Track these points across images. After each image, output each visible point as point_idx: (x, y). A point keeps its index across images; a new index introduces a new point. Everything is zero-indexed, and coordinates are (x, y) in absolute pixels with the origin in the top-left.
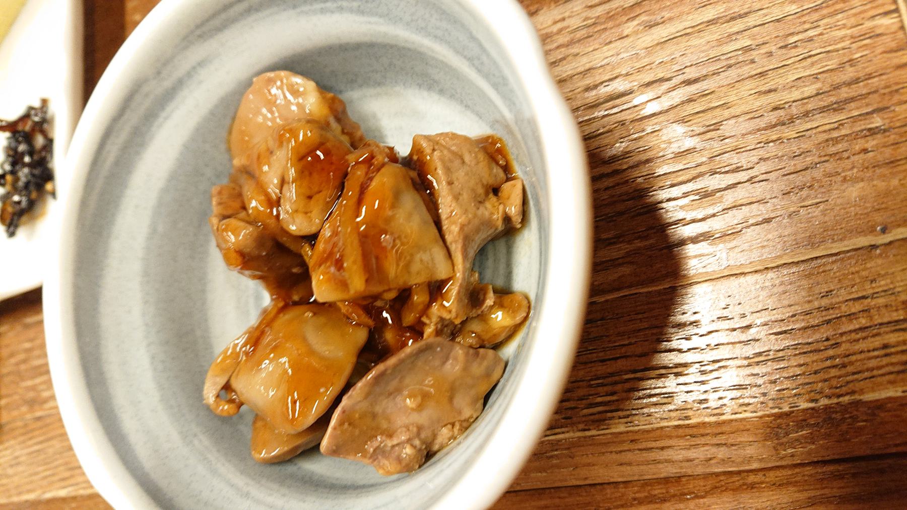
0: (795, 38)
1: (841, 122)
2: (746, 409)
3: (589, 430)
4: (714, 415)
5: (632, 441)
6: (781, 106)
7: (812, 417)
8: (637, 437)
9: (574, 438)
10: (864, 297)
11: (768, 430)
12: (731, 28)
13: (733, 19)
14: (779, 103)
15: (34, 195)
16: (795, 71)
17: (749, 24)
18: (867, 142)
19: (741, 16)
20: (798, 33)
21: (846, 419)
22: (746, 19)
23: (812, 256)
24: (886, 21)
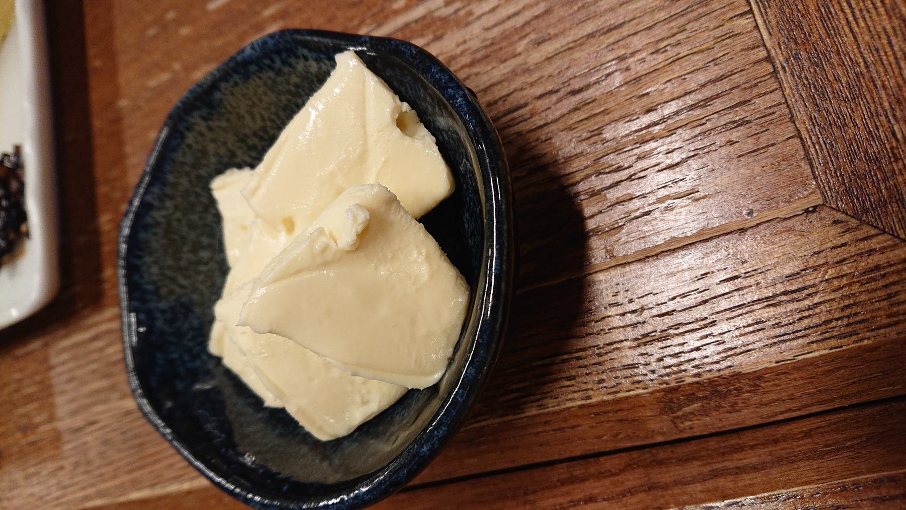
0: (665, 43)
1: (707, 118)
2: (638, 386)
3: (507, 415)
4: (611, 393)
5: (545, 423)
6: (654, 108)
7: (699, 390)
8: (549, 419)
9: (563, 483)
10: (736, 277)
11: (662, 405)
12: (607, 39)
13: (610, 30)
14: (651, 105)
15: (12, 236)
16: (665, 74)
17: (623, 35)
18: (731, 134)
19: (616, 28)
20: (667, 38)
21: (731, 390)
22: (621, 30)
23: (686, 243)
24: (743, 22)
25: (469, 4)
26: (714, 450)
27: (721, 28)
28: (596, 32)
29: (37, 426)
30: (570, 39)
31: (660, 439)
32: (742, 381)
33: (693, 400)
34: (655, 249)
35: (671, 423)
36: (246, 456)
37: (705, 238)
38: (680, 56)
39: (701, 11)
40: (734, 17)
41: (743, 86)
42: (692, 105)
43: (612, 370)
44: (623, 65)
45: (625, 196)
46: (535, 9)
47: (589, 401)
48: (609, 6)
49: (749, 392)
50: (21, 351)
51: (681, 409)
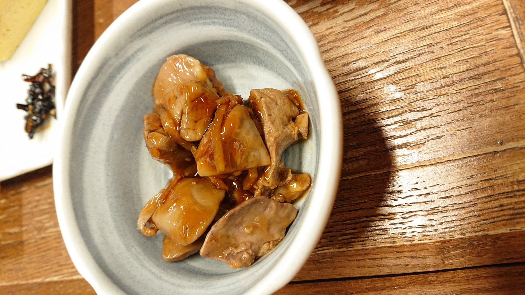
0: (456, 40)
1: (479, 85)
6: (448, 76)
7: (462, 243)
8: (368, 252)
13: (423, 29)
14: (447, 74)
17: (431, 32)
21: (480, 244)
22: (430, 29)
24: (504, 32)
25: (336, 6)
26: (462, 277)
27: (490, 35)
28: (415, 28)
29: (47, 228)
30: (398, 31)
31: (432, 269)
32: (488, 239)
33: (457, 248)
34: (444, 159)
35: (441, 260)
36: (145, 115)
37: (474, 155)
38: (465, 48)
39: (479, 23)
40: (499, 29)
41: (502, 69)
42: (471, 77)
43: (410, 227)
44: (431, 49)
45: (427, 126)
46: (378, 12)
47: (395, 244)
48: (423, 15)
49: (490, 246)
50: (40, 184)
51: (449, 253)
